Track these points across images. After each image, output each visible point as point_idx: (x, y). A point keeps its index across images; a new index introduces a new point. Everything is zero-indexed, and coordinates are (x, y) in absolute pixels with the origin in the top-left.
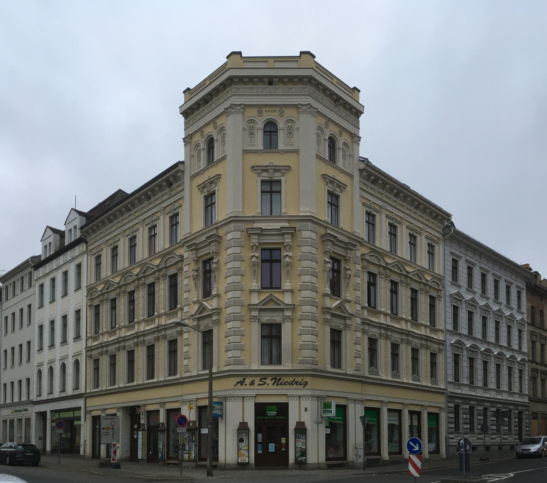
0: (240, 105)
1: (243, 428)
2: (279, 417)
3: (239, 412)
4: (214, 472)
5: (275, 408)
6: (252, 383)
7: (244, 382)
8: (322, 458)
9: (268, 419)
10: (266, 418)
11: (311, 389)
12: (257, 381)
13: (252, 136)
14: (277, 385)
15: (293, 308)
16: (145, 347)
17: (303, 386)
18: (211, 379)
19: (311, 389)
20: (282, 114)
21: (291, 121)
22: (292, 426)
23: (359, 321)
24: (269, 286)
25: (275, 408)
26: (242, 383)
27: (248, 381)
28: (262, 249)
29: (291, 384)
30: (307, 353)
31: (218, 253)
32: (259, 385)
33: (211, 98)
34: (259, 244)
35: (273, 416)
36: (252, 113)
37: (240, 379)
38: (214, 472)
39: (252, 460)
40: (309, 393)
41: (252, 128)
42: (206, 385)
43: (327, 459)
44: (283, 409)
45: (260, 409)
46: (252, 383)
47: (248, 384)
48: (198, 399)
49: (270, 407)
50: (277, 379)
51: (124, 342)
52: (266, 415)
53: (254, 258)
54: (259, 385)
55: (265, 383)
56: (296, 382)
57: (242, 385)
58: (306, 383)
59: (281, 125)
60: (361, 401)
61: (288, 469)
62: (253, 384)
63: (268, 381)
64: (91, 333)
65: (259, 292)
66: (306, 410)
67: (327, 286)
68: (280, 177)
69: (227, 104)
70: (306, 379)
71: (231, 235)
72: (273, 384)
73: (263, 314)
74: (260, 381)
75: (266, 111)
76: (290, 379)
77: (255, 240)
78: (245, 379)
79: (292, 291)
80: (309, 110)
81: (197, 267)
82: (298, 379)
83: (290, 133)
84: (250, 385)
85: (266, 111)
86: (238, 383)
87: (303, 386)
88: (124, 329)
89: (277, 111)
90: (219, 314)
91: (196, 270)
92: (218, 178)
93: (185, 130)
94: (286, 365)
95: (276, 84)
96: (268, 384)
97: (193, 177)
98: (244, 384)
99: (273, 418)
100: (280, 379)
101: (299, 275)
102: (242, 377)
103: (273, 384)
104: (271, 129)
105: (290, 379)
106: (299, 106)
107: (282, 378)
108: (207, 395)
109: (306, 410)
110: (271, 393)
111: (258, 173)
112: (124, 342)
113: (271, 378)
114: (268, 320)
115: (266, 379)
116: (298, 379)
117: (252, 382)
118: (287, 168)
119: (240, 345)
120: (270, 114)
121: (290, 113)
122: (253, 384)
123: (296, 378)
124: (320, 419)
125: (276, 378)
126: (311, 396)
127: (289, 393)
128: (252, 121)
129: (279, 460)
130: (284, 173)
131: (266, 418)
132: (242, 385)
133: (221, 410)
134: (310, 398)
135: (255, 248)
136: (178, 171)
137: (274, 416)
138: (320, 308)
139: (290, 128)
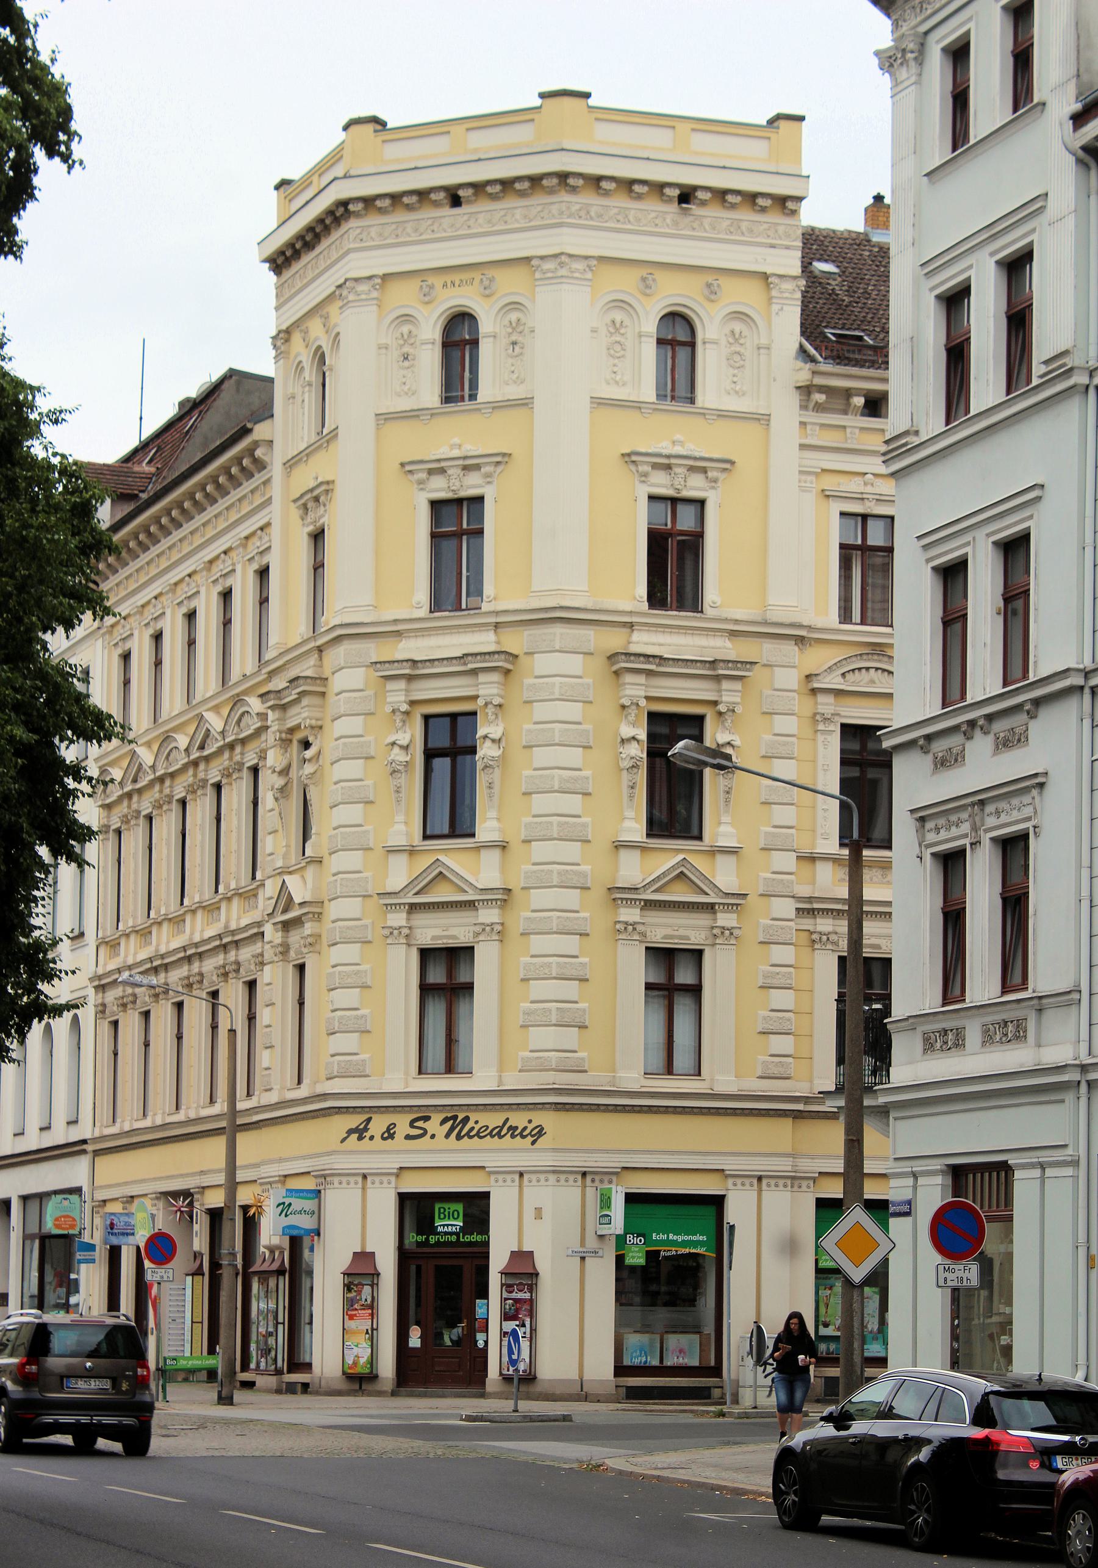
0: (370, 278)
1: (360, 1273)
2: (468, 1238)
3: (361, 1226)
4: (239, 1396)
5: (460, 1207)
6: (389, 1134)
7: (366, 1129)
8: (600, 1367)
9: (438, 1244)
10: (433, 1239)
11: (554, 1150)
12: (403, 1127)
13: (406, 363)
14: (459, 1137)
15: (504, 897)
16: (241, 985)
17: (530, 1139)
18: (233, 1127)
19: (554, 1150)
20: (488, 293)
21: (515, 306)
22: (498, 1261)
23: (786, 908)
24: (446, 831)
25: (460, 1207)
26: (360, 1132)
27: (378, 1125)
28: (427, 718)
29: (497, 1133)
30: (545, 1037)
31: (321, 727)
32: (408, 1137)
33: (317, 238)
34: (412, 703)
35: (451, 1234)
36: (404, 296)
37: (355, 1121)
38: (239, 1396)
39: (387, 1367)
40: (547, 1160)
41: (408, 339)
42: (219, 1144)
43: (621, 1370)
44: (476, 1207)
45: (416, 1209)
46: (389, 1134)
47: (378, 1138)
48: (285, 1176)
49: (446, 1206)
50: (457, 1123)
51: (166, 971)
52: (433, 1230)
53: (396, 750)
54: (408, 1137)
55: (425, 1132)
56: (510, 1128)
57: (360, 1138)
58: (540, 1132)
59: (486, 326)
60: (794, 1180)
61: (483, 1395)
62: (391, 1136)
63: (433, 1125)
64: (104, 930)
65: (412, 852)
66: (539, 1213)
67: (632, 814)
68: (481, 486)
69: (335, 276)
70: (540, 1118)
71: (348, 676)
72: (447, 1136)
73: (421, 919)
74: (412, 1125)
75: (445, 285)
76: (493, 1120)
77: (397, 695)
78: (369, 1120)
79: (503, 847)
80: (563, 272)
81: (285, 763)
82: (518, 1120)
83: (514, 343)
84: (383, 1139)
85: (445, 285)
86: (350, 1132)
87: (530, 1139)
88: (235, 901)
89: (477, 282)
90: (318, 917)
91: (281, 773)
92: (327, 491)
93: (277, 309)
94: (483, 1075)
95: (469, 202)
96: (433, 1136)
97: (291, 464)
98: (368, 1134)
99: (454, 1238)
100: (466, 1119)
101: (524, 794)
102: (363, 1117)
103: (447, 1136)
104: (459, 339)
105: (493, 1120)
106: (534, 262)
107: (473, 1118)
108: (221, 1179)
109: (539, 1213)
110: (442, 1164)
111: (420, 482)
112: (166, 971)
113: (442, 1116)
114: (433, 938)
115: (427, 1119)
116: (518, 1120)
117: (388, 1130)
118: (499, 459)
119: (357, 1017)
120: (456, 291)
121: (510, 284)
122: (391, 1136)
123: (514, 1117)
124: (592, 1243)
125: (455, 1118)
126: (554, 1172)
127: (491, 1161)
128: (406, 319)
129: (464, 1370)
130: (488, 475)
131: (433, 1239)
132: (360, 1138)
133: (318, 1213)
134: (552, 1178)
135: (398, 718)
136: (256, 444)
137: (457, 1234)
138: (598, 893)
139: (516, 327)
